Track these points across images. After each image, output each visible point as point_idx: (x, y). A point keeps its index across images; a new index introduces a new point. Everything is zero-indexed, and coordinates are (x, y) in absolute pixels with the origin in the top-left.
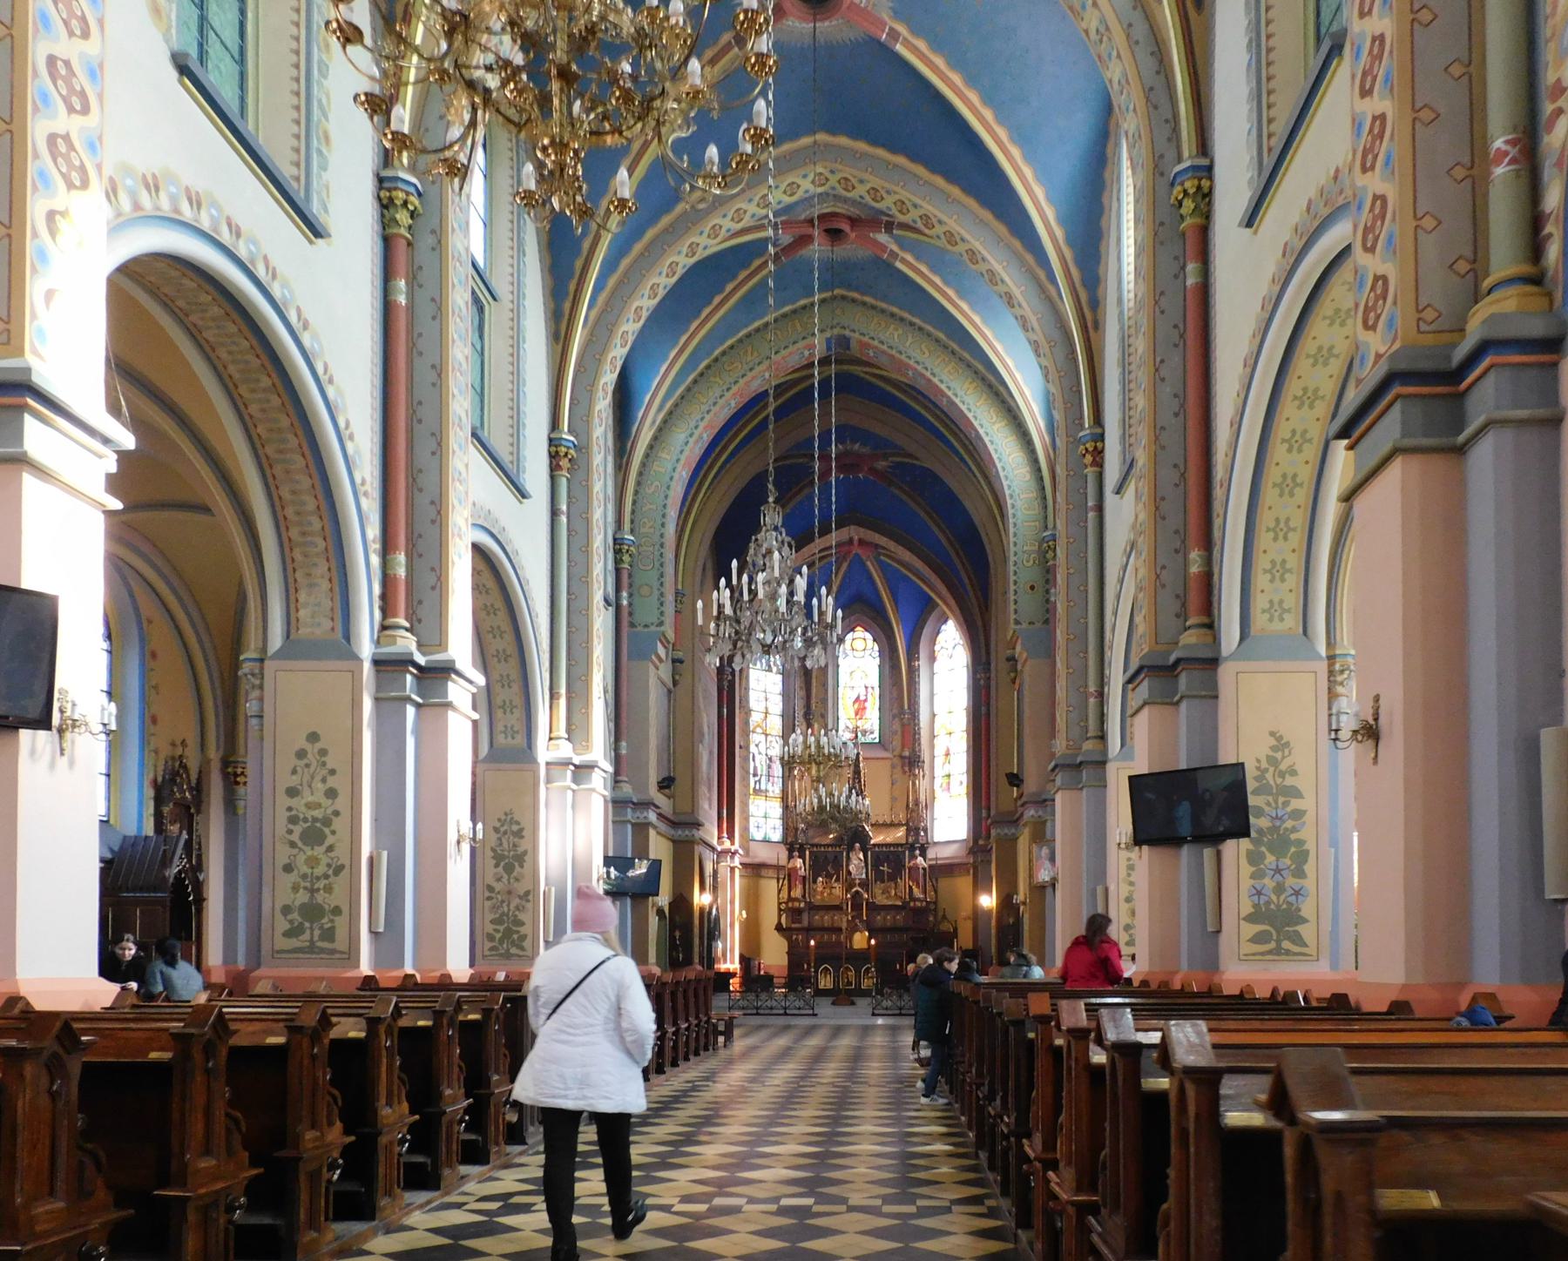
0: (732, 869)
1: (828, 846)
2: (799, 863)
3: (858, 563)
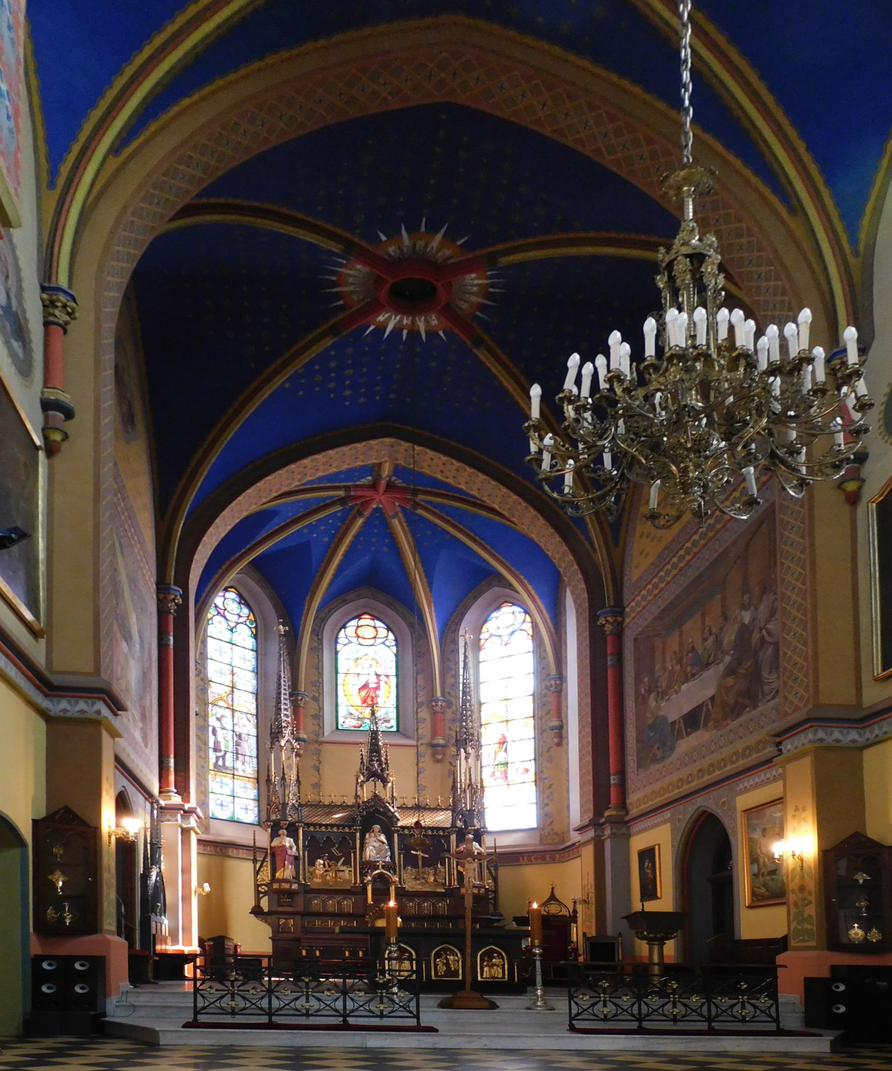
0: (186, 832)
1: (332, 826)
2: (288, 842)
3: (380, 520)
